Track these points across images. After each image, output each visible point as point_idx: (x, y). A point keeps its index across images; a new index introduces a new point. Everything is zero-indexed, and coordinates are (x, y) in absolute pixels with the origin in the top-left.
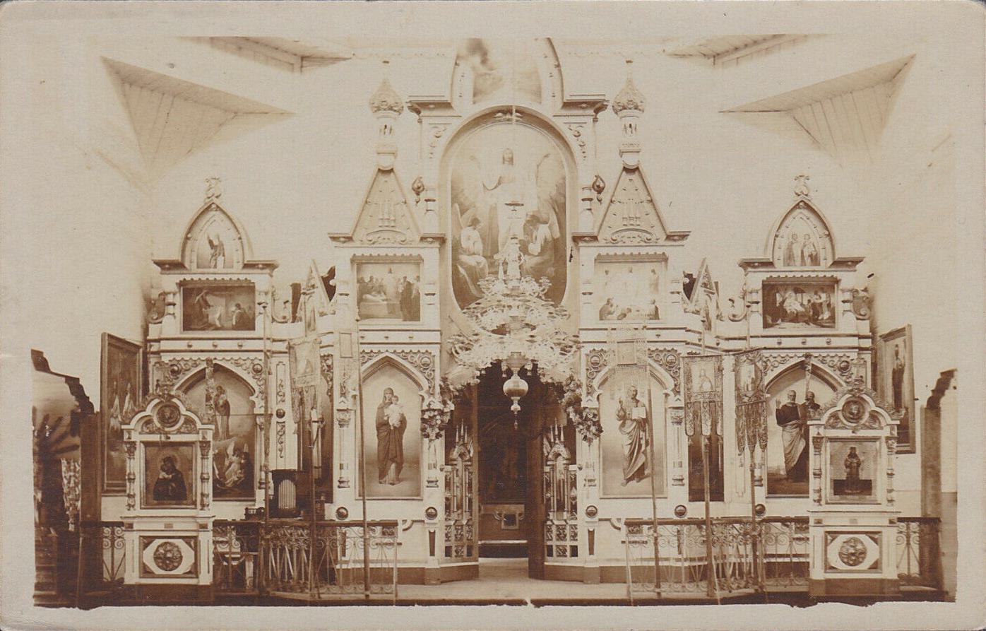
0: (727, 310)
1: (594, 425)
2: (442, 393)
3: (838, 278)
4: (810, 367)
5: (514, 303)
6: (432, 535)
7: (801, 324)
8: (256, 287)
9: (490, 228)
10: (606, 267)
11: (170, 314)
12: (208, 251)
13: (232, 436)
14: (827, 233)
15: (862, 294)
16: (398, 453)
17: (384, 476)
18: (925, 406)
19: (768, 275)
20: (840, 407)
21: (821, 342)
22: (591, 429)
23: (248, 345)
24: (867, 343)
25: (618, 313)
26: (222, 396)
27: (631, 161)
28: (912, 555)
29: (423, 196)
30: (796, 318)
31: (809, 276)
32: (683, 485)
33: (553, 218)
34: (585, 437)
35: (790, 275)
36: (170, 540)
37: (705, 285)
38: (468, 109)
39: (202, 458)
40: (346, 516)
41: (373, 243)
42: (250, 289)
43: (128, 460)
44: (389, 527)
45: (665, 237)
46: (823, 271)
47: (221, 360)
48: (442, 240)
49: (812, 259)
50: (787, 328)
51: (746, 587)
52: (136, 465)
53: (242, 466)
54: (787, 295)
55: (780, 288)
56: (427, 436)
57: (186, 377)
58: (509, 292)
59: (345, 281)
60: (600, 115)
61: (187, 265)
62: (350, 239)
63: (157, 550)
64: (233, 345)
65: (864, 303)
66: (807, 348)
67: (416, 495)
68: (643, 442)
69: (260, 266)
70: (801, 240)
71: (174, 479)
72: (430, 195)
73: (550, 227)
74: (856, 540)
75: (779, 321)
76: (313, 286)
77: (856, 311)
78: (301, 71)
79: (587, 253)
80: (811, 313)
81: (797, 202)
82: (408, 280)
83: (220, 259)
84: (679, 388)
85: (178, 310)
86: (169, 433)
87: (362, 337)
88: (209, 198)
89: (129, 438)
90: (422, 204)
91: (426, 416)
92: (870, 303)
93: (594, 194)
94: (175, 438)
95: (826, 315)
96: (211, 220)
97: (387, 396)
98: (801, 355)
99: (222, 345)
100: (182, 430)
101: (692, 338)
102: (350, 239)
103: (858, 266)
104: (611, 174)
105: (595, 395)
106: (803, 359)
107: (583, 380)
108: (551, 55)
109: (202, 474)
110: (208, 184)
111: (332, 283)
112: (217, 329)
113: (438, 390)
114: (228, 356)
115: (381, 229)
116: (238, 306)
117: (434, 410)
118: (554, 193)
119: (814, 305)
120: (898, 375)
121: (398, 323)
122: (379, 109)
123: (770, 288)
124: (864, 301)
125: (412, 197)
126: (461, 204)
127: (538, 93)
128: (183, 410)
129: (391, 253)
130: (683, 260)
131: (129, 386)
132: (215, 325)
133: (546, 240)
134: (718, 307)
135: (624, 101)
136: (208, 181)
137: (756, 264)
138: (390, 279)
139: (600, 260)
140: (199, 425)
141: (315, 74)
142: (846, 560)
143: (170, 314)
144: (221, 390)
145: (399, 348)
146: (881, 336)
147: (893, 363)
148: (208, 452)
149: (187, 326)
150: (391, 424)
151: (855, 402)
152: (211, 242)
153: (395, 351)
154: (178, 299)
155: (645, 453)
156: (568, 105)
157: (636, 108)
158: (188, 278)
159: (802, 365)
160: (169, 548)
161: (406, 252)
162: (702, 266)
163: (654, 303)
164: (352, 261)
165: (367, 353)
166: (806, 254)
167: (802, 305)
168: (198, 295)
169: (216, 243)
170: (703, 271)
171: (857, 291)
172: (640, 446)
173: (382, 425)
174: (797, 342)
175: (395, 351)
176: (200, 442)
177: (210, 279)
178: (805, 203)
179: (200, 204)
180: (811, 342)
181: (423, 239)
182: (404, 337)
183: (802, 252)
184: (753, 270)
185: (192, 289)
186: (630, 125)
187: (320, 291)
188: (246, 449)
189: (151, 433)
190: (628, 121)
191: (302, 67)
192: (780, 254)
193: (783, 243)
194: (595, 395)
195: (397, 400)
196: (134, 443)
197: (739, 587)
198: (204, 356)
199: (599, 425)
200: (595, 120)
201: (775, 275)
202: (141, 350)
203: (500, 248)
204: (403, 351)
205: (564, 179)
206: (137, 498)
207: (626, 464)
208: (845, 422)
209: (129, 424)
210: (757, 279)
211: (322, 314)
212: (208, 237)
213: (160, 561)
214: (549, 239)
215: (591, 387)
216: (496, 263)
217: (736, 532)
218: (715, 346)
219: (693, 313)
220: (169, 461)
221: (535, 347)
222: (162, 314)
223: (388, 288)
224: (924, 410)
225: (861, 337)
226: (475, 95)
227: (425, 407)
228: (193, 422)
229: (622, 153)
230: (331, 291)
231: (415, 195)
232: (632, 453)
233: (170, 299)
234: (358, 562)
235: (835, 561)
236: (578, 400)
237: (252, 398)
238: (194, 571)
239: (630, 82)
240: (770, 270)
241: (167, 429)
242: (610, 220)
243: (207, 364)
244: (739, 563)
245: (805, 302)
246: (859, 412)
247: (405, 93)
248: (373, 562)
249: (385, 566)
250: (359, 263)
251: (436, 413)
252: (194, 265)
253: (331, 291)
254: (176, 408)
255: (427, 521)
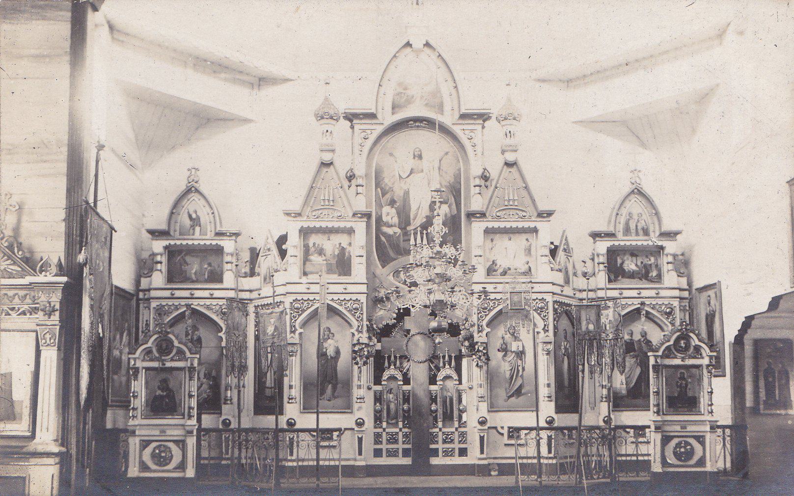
0: (580, 268)
1: (484, 355)
2: (368, 331)
3: (664, 246)
4: (644, 312)
5: (437, 263)
6: (360, 440)
7: (636, 279)
8: (225, 249)
9: (404, 206)
10: (492, 236)
11: (158, 270)
12: (187, 222)
13: (203, 364)
14: (654, 212)
15: (681, 257)
16: (334, 375)
17: (323, 394)
18: (733, 342)
19: (611, 243)
20: (671, 343)
21: (652, 293)
22: (482, 358)
23: (217, 294)
24: (686, 294)
25: (500, 270)
26: (196, 332)
27: (510, 157)
28: (727, 452)
29: (354, 182)
30: (632, 275)
31: (199, 244)
32: (551, 401)
33: (452, 200)
34: (477, 364)
35: (628, 243)
36: (163, 443)
37: (565, 250)
38: (388, 119)
39: (190, 380)
40: (295, 424)
41: (317, 218)
42: (218, 251)
43: (133, 381)
44: (325, 434)
45: (536, 214)
46: (654, 240)
47: (197, 305)
48: (368, 216)
49: (644, 232)
50: (625, 283)
51: (604, 477)
52: (139, 386)
53: (210, 387)
54: (625, 258)
55: (620, 253)
56: (357, 363)
57: (170, 318)
58: (434, 256)
59: (294, 244)
60: (487, 124)
61: (172, 233)
62: (300, 215)
63: (154, 451)
64: (206, 294)
65: (683, 265)
66: (642, 298)
67: (347, 408)
68: (520, 368)
69: (603, 235)
70: (635, 217)
71: (167, 396)
72: (360, 182)
73: (450, 207)
74: (687, 443)
75: (620, 278)
76: (269, 250)
77: (676, 270)
78: (259, 88)
79: (478, 227)
80: (644, 272)
81: (632, 189)
82: (342, 245)
83: (197, 229)
84: (548, 327)
85: (163, 267)
86: (165, 360)
87: (532, 288)
88: (190, 183)
89: (134, 364)
90: (353, 188)
91: (356, 349)
92: (686, 263)
93: (482, 183)
94: (168, 364)
95: (654, 273)
96: (192, 199)
97: (326, 333)
98: (637, 303)
99: (198, 294)
100: (175, 358)
101: (557, 289)
102: (300, 215)
103: (678, 237)
104: (495, 168)
105: (485, 333)
106: (639, 306)
107: (474, 318)
108: (450, 79)
109: (190, 392)
110: (189, 172)
111: (284, 247)
112: (193, 282)
113: (365, 329)
114: (202, 302)
115: (322, 207)
116: (210, 265)
117: (363, 344)
118: (452, 180)
119: (645, 266)
120: (710, 319)
121: (335, 278)
122: (322, 118)
123: (612, 253)
124: (682, 263)
125: (346, 183)
126: (382, 189)
127: (440, 108)
128: (176, 343)
129: (330, 225)
130: (548, 233)
131: (126, 325)
132: (192, 279)
133: (446, 215)
134: (574, 267)
135: (504, 114)
136: (189, 170)
137: (603, 235)
138: (330, 245)
139: (488, 231)
140: (188, 355)
141: (269, 91)
142: (168, 461)
143: (158, 270)
144: (195, 328)
145: (336, 297)
146: (696, 289)
147: (706, 309)
148: (194, 375)
149: (170, 279)
150: (328, 354)
151: (683, 339)
152: (190, 216)
153: (333, 299)
154: (164, 259)
155: (522, 376)
156: (463, 116)
157: (514, 119)
158: (172, 242)
159: (638, 311)
160: (162, 449)
161: (342, 225)
162: (562, 236)
163: (528, 264)
164: (300, 231)
165: (306, 300)
166: (639, 228)
167: (636, 265)
168: (179, 255)
169: (194, 216)
170: (564, 239)
171: (677, 255)
172: (518, 371)
173: (322, 355)
174: (634, 293)
175: (333, 299)
176: (188, 367)
177: (189, 243)
178: (638, 190)
179: (183, 187)
180: (645, 293)
181: (354, 215)
182: (339, 288)
183: (637, 226)
184: (601, 239)
185: (175, 251)
186: (510, 132)
187: (275, 251)
188: (214, 373)
189: (151, 360)
190: (326, 127)
191: (259, 85)
192: (621, 227)
193: (623, 220)
194: (485, 333)
195: (334, 336)
196: (138, 368)
197: (598, 478)
198: (183, 302)
199: (488, 355)
200: (483, 127)
201: (617, 243)
202: (135, 298)
203: (412, 221)
204: (339, 299)
205: (459, 170)
206: (139, 410)
207: (507, 385)
208: (676, 353)
209: (657, 352)
210: (603, 246)
211: (277, 271)
212: (188, 212)
213: (156, 459)
214: (449, 215)
215: (294, 326)
216: (409, 233)
217: (596, 436)
218: (573, 295)
219: (557, 271)
220: (165, 381)
221: (463, 299)
222: (151, 270)
223: (327, 252)
224: (732, 345)
225: (681, 290)
226: (393, 108)
227: (355, 342)
228: (183, 353)
229: (503, 152)
230: (283, 254)
231: (348, 182)
232: (512, 378)
233: (159, 258)
234: (312, 460)
235: (671, 459)
236: (472, 337)
237: (220, 334)
238: (182, 466)
239: (509, 100)
240: (613, 239)
241: (163, 358)
242: (495, 200)
243: (187, 308)
244: (599, 461)
245: (639, 264)
246: (686, 346)
247: (342, 106)
248: (325, 460)
249: (332, 463)
250: (305, 233)
251: (363, 346)
252: (177, 233)
253: (283, 254)
254: (172, 342)
255: (356, 429)
